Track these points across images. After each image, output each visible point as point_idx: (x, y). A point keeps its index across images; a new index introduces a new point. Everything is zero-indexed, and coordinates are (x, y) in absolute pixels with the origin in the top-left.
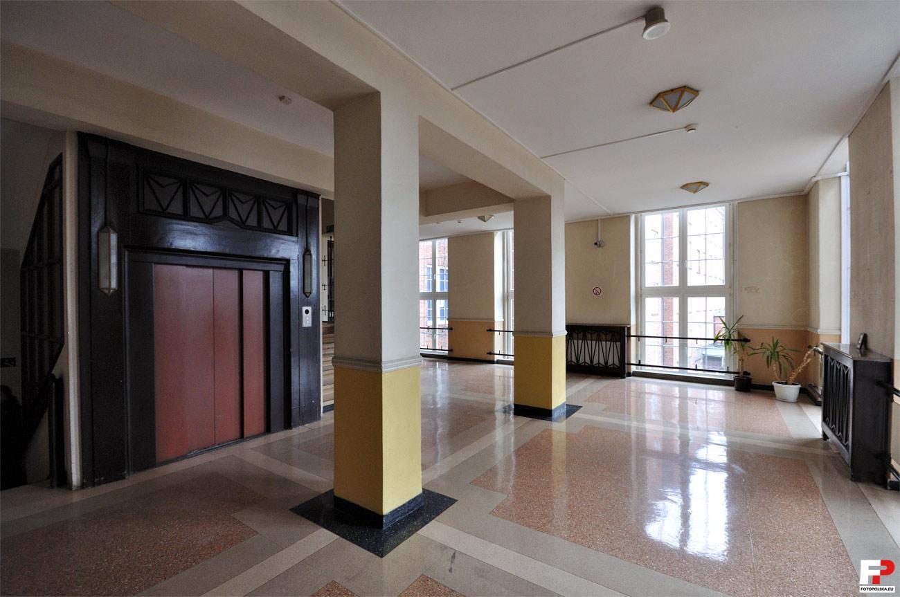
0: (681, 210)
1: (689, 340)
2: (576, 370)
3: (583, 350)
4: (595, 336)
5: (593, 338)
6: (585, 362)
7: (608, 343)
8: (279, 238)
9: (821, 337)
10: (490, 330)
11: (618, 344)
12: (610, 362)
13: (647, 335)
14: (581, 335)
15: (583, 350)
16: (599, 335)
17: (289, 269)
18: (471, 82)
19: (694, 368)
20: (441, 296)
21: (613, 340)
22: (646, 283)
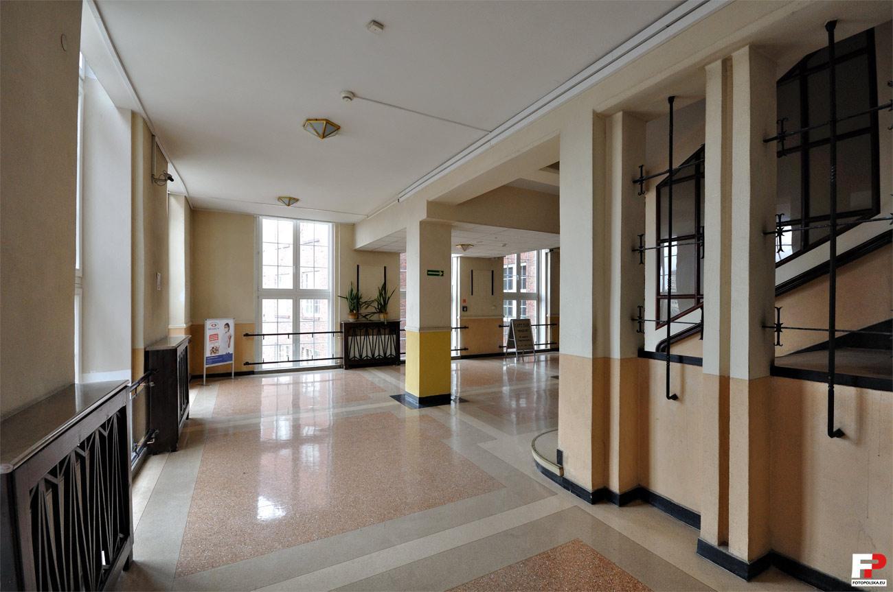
0: (295, 221)
1: (301, 335)
2: (467, 355)
3: (386, 341)
4: (375, 331)
5: (386, 333)
6: (355, 357)
7: (363, 337)
8: (789, 351)
9: (172, 332)
10: (465, 328)
11: (395, 336)
12: (388, 353)
13: (301, 332)
14: (375, 331)
15: (386, 341)
16: (367, 331)
17: (805, 349)
18: (374, 101)
19: (331, 357)
20: (511, 297)
21: (391, 333)
22: (828, 335)
